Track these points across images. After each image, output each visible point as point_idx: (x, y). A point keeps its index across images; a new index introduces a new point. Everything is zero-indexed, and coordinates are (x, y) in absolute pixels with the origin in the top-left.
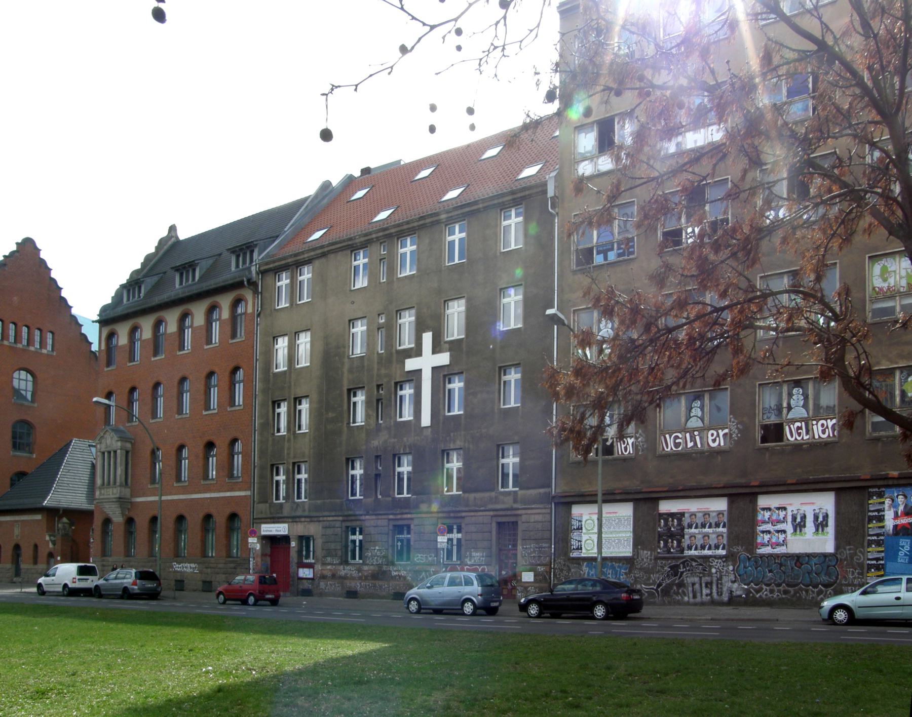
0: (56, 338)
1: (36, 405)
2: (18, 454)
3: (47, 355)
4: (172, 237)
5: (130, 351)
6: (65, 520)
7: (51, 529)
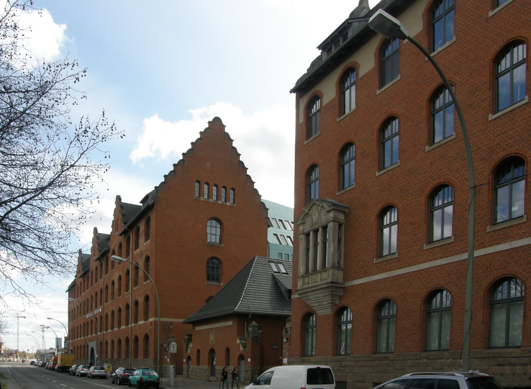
0: (236, 193)
1: (223, 245)
2: (211, 283)
3: (231, 207)
4: (364, 8)
5: (340, 104)
6: (254, 323)
7: (241, 334)
